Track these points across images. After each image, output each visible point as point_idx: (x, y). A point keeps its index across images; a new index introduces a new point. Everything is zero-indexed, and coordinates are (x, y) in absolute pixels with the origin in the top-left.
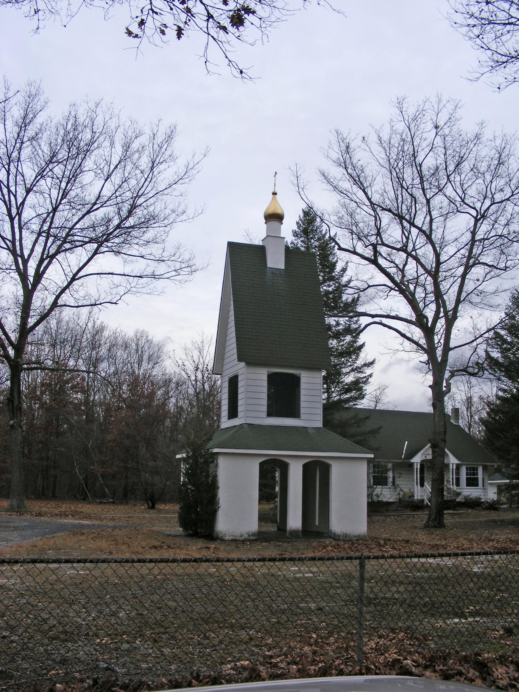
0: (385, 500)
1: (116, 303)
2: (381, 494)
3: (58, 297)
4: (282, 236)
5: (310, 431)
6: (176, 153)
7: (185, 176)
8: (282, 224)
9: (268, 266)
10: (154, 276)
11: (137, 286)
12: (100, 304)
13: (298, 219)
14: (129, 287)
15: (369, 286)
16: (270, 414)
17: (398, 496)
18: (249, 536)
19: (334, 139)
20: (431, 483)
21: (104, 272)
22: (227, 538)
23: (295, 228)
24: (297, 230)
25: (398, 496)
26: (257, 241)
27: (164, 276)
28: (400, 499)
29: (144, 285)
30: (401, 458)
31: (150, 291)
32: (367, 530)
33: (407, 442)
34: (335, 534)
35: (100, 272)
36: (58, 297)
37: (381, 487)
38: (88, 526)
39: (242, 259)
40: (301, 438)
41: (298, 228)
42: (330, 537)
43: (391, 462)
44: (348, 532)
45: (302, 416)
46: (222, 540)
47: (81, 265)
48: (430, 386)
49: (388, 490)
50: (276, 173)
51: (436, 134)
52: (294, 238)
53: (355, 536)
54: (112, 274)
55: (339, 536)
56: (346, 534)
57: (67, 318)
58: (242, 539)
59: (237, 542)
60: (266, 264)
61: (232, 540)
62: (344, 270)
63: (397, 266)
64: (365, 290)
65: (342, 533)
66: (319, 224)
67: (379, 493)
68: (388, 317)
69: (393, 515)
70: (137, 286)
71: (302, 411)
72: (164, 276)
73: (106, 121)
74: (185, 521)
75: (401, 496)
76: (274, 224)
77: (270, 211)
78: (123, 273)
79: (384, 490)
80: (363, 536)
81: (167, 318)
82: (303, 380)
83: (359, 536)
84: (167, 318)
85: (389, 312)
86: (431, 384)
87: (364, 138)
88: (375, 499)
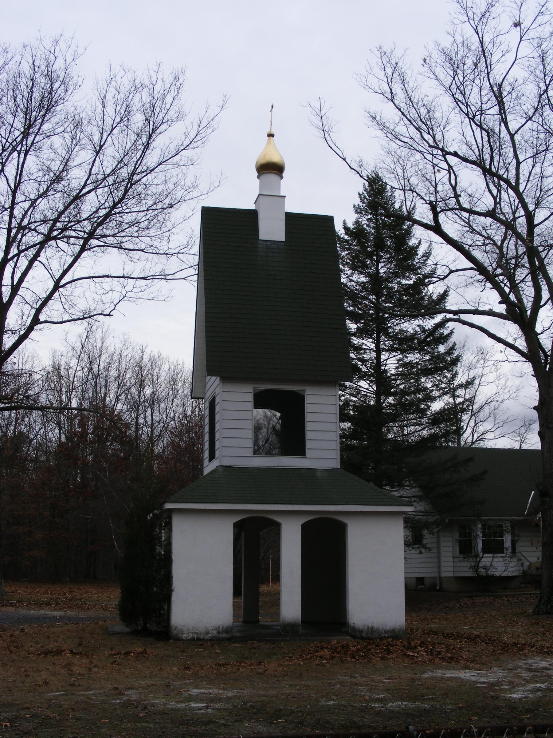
0: (497, 574)
1: (109, 315)
2: (491, 565)
3: (39, 311)
4: (282, 194)
5: (319, 474)
6: (186, 109)
7: (198, 138)
8: (282, 178)
9: (260, 238)
10: (164, 277)
11: (134, 290)
12: (90, 317)
13: (361, 190)
14: (124, 293)
15: (451, 272)
16: (256, 452)
17: (521, 569)
18: (219, 633)
19: (375, 60)
20: (540, 549)
21: (97, 275)
22: (184, 636)
23: (358, 202)
24: (361, 204)
25: (521, 569)
26: (250, 205)
27: (178, 276)
28: (523, 571)
29: (143, 288)
30: (523, 515)
31: (153, 295)
32: (406, 620)
33: (533, 492)
34: (354, 629)
35: (91, 275)
36: (39, 311)
37: (491, 555)
38: (61, 618)
39: (225, 230)
40: (304, 485)
41: (362, 201)
42: (348, 634)
43: (508, 520)
44: (375, 626)
45: (308, 453)
46: (177, 639)
47: (66, 267)
48: (535, 408)
49: (502, 559)
50: (272, 106)
51: (521, 38)
52: (356, 215)
53: (386, 632)
54: (107, 276)
55: (361, 631)
56: (372, 628)
57: (111, 349)
58: (207, 637)
59: (202, 642)
60: (257, 235)
61: (193, 639)
62: (427, 255)
63: (495, 244)
64: (446, 277)
65: (366, 628)
66: (390, 194)
67: (488, 564)
68: (476, 312)
69: (506, 596)
70: (134, 290)
71: (309, 445)
72: (178, 276)
73: (68, 63)
74: (129, 611)
75: (525, 568)
76: (271, 177)
77: (264, 161)
78: (122, 275)
79: (495, 559)
80: (399, 631)
81: (135, 322)
82: (309, 400)
83: (393, 631)
84: (135, 322)
85: (477, 305)
86: (537, 405)
87: (425, 61)
88: (482, 572)
